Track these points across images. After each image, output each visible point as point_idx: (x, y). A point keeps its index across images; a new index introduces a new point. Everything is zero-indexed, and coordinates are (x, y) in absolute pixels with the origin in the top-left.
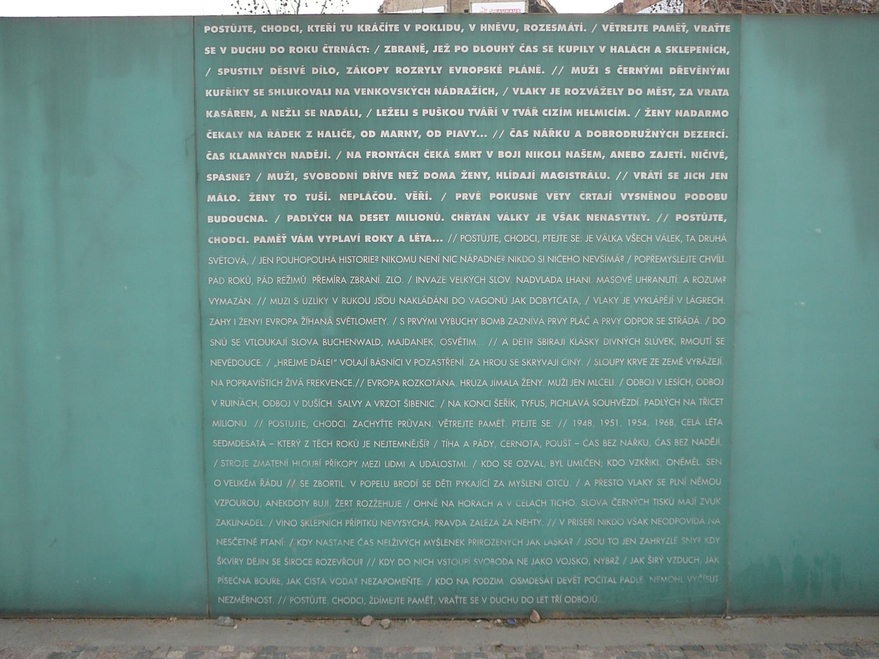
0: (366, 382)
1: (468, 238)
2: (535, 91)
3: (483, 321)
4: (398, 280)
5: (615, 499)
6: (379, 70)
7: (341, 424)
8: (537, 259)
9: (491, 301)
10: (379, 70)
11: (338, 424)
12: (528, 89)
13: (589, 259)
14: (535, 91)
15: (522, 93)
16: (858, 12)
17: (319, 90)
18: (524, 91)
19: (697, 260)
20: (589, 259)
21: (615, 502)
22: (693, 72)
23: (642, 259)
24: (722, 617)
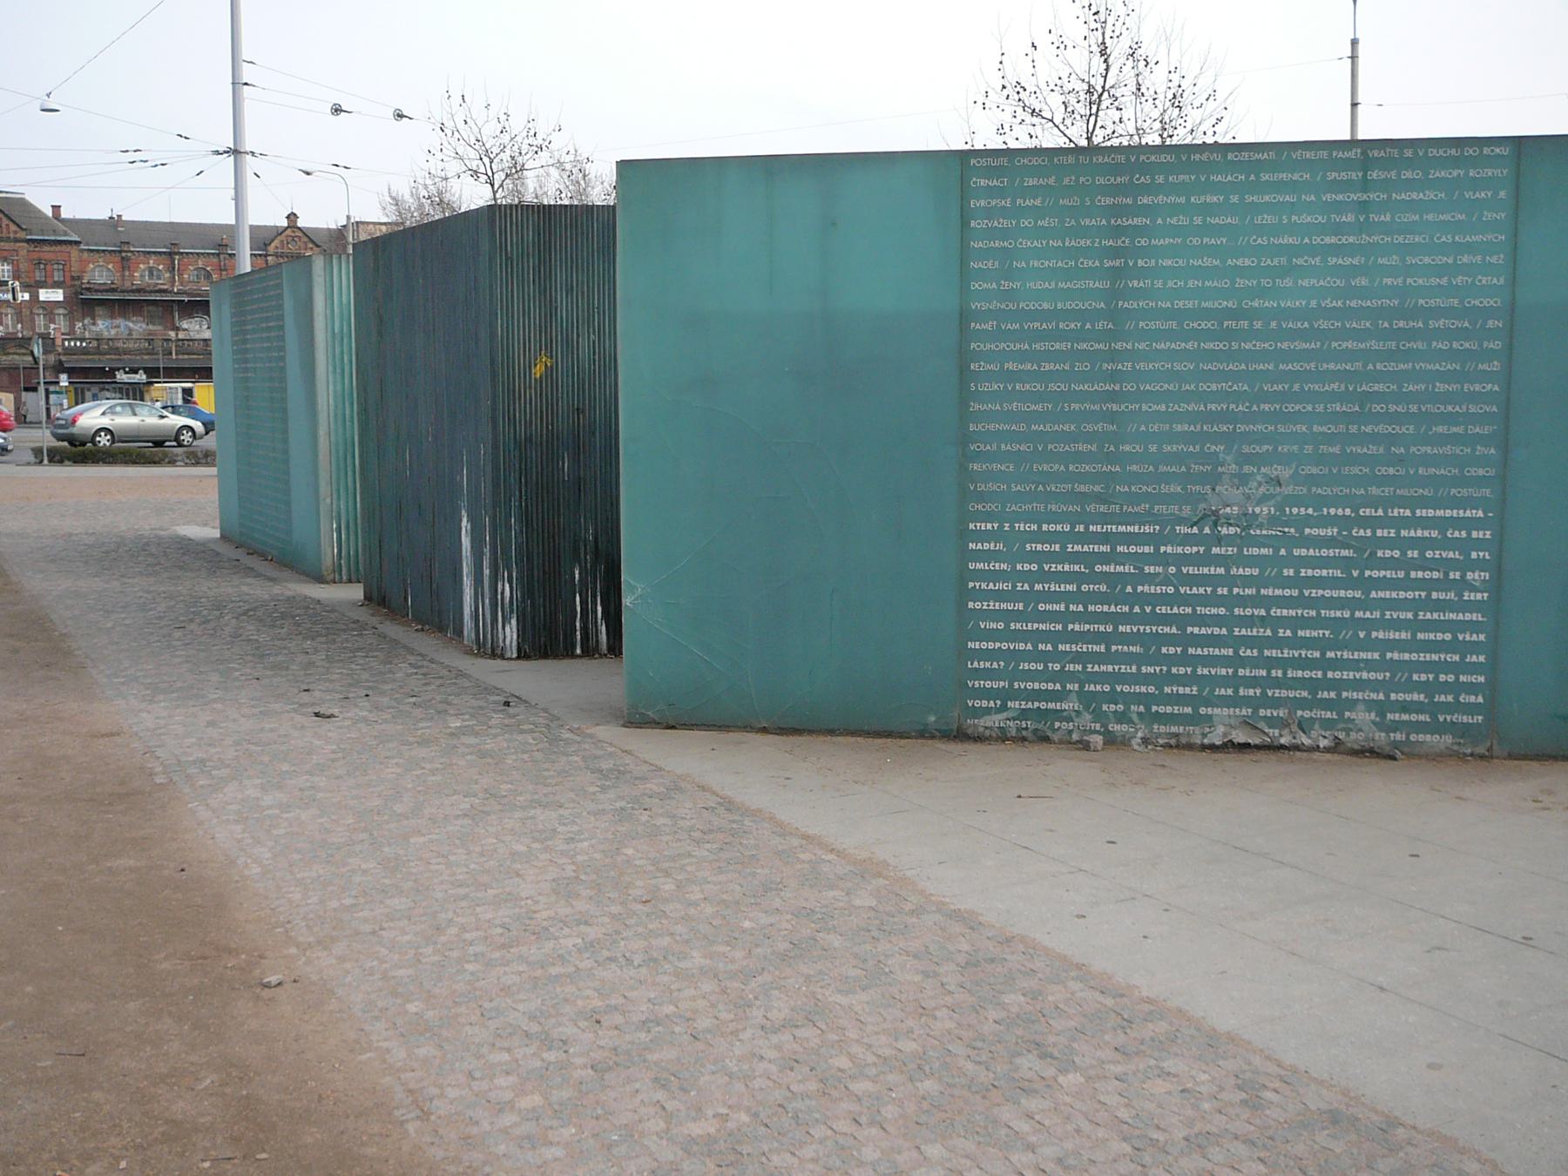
0: (1032, 467)
1: (1147, 325)
2: (1202, 591)
3: (1145, 408)
4: (1086, 366)
5: (1480, 277)
6: (1195, 549)
7: (1213, 325)
8: (1231, 346)
9: (1161, 387)
10: (1195, 549)
11: (1209, 325)
12: (1195, 588)
13: (1285, 346)
14: (1202, 591)
15: (1188, 592)
16: (1024, 739)
17: (1451, 553)
18: (1191, 590)
19: (1398, 347)
20: (1285, 346)
21: (1480, 281)
22: (1275, 714)
23: (1340, 345)
24: (625, 709)
